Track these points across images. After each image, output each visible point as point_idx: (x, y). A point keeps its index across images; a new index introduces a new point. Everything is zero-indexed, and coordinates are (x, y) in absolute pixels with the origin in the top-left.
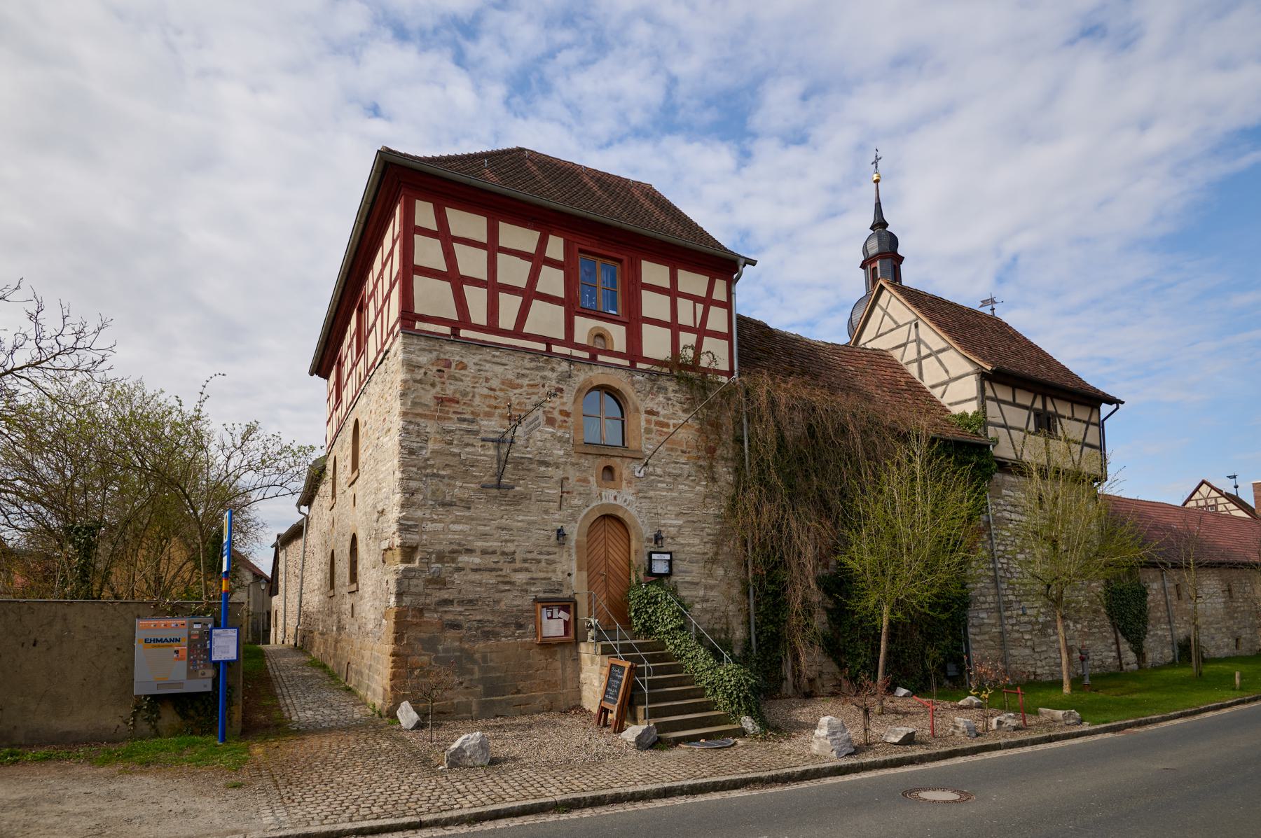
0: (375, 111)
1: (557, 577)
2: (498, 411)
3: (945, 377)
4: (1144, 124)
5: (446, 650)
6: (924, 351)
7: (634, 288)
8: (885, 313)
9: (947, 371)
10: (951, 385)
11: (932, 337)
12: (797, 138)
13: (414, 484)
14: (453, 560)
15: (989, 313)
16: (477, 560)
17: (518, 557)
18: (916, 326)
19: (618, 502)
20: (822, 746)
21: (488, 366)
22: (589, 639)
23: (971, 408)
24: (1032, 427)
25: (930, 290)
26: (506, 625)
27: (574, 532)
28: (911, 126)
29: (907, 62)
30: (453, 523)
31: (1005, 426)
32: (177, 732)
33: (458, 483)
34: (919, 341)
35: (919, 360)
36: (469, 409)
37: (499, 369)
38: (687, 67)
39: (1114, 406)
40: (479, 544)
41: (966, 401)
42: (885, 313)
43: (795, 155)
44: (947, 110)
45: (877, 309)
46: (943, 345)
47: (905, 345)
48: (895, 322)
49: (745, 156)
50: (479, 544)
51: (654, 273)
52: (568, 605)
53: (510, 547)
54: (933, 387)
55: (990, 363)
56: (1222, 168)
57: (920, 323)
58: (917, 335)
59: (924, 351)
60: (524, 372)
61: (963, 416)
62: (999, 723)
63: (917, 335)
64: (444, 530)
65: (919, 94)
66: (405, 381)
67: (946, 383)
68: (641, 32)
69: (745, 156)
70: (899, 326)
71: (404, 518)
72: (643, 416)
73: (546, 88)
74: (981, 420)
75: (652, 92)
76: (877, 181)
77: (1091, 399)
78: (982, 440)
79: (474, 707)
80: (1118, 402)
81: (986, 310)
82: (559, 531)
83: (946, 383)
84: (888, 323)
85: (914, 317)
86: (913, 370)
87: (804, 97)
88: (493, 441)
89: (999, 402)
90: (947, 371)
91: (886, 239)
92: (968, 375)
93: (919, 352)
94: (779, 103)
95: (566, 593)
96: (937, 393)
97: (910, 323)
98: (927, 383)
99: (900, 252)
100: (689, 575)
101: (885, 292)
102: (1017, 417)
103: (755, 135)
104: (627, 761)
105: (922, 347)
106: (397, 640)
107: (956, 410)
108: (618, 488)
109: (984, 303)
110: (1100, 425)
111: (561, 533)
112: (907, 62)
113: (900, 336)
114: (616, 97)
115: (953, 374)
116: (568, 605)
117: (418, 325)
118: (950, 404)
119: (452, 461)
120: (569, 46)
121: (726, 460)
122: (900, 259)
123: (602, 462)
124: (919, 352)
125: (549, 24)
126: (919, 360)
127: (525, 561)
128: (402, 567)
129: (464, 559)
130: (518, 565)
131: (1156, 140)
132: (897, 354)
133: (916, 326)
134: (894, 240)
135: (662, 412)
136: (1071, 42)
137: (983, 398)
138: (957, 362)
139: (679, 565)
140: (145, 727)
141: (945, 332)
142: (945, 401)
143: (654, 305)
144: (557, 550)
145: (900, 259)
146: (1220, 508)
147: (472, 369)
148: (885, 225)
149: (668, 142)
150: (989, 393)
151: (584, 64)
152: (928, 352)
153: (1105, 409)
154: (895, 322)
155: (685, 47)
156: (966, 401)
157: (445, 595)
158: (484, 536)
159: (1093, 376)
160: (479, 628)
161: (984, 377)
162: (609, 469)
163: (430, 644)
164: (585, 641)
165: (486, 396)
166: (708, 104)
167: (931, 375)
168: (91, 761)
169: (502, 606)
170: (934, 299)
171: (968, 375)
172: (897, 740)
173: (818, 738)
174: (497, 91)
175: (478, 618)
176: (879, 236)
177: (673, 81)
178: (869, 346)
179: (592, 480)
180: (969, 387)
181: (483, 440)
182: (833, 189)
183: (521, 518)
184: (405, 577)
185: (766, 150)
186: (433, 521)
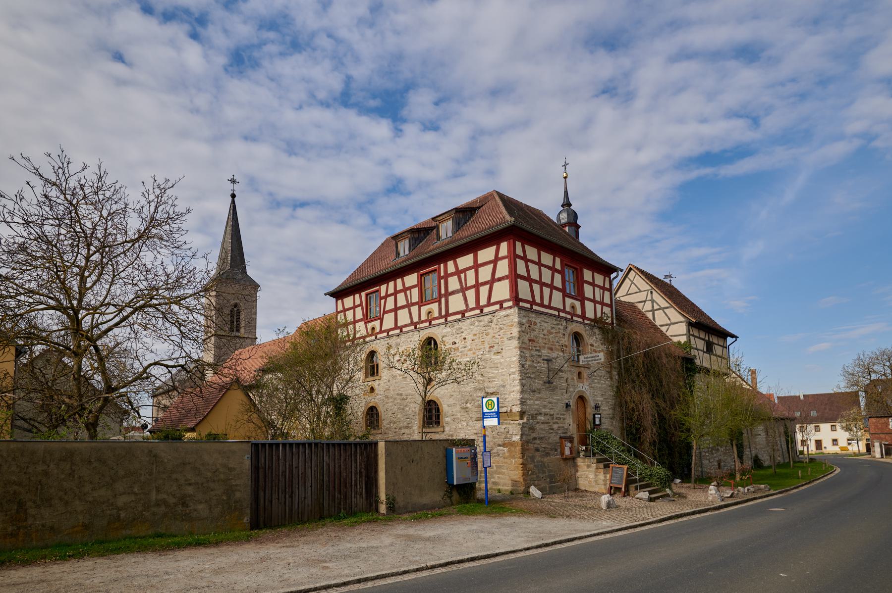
0: (119, 57)
1: (566, 426)
3: (669, 322)
4: (638, 148)
6: (656, 307)
7: (580, 283)
8: (632, 282)
11: (660, 300)
12: (431, 126)
13: (524, 382)
23: (683, 339)
25: (648, 272)
26: (552, 449)
27: (572, 403)
28: (502, 130)
29: (499, 92)
31: (696, 349)
32: (459, 503)
34: (653, 301)
35: (653, 311)
37: (546, 325)
38: (360, 73)
42: (632, 282)
43: (430, 137)
44: (525, 124)
46: (668, 305)
47: (644, 302)
49: (398, 132)
51: (587, 275)
52: (571, 439)
53: (552, 412)
54: (661, 326)
55: (694, 318)
56: (680, 177)
59: (656, 307)
61: (679, 342)
64: (535, 403)
65: (505, 112)
67: (669, 325)
68: (323, 42)
69: (398, 132)
70: (641, 291)
73: (255, 64)
74: (687, 346)
75: (336, 83)
78: (689, 356)
80: (737, 337)
81: (667, 281)
83: (669, 325)
86: (650, 315)
87: (436, 104)
89: (695, 336)
94: (421, 103)
95: (569, 434)
96: (664, 329)
100: (606, 425)
103: (404, 121)
107: (675, 339)
108: (583, 382)
109: (666, 277)
110: (727, 348)
111: (568, 405)
112: (499, 92)
113: (642, 296)
114: (306, 80)
115: (673, 320)
120: (273, 42)
124: (653, 307)
125: (261, 27)
126: (653, 311)
129: (539, 417)
130: (555, 420)
131: (644, 157)
132: (640, 306)
136: (597, 96)
137: (689, 335)
138: (674, 315)
139: (603, 420)
140: (448, 501)
142: (668, 334)
143: (588, 291)
146: (738, 384)
147: (539, 325)
149: (343, 111)
151: (282, 54)
153: (730, 340)
155: (357, 60)
157: (534, 435)
158: (545, 406)
159: (723, 322)
161: (690, 324)
162: (580, 373)
166: (374, 97)
167: (660, 319)
169: (550, 441)
174: (221, 60)
177: (349, 80)
178: (622, 299)
180: (682, 328)
182: (457, 161)
185: (411, 130)
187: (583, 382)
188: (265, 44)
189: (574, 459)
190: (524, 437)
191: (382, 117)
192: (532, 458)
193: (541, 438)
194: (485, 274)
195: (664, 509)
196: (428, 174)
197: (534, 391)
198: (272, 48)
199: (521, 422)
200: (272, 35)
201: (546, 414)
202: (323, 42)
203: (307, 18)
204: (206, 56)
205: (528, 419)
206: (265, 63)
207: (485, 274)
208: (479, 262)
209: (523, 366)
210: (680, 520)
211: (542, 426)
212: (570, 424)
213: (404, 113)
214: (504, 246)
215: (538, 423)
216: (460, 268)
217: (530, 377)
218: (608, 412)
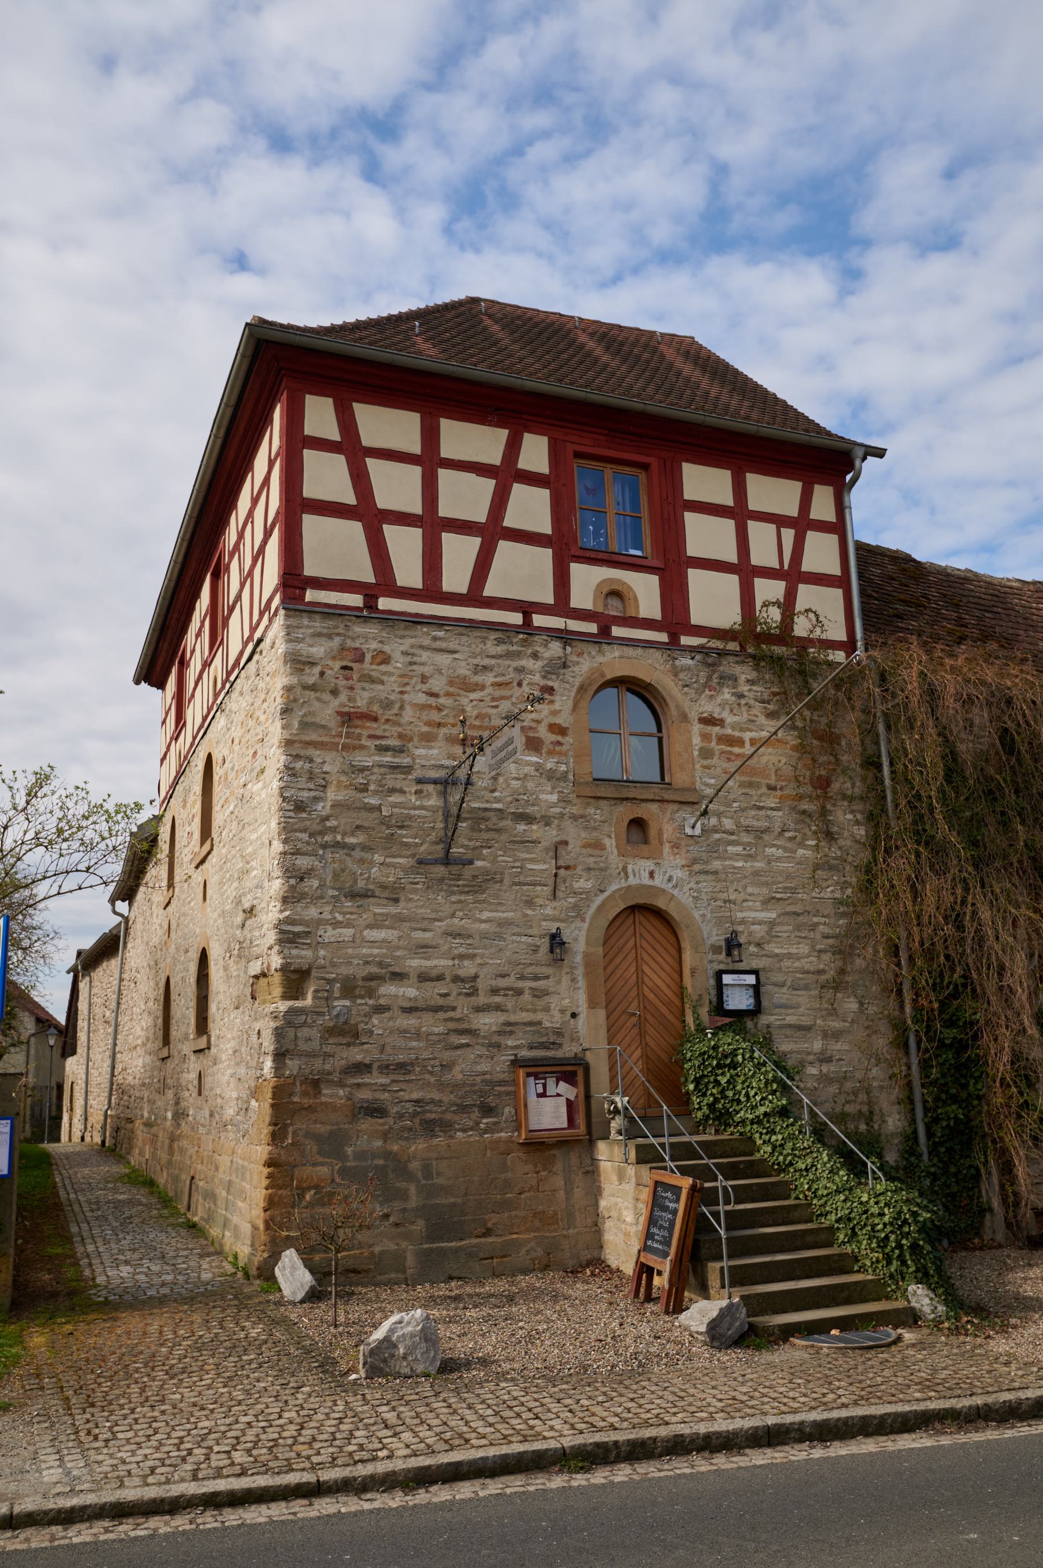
1: (552, 1020)
12: (942, 239)
13: (303, 862)
26: (463, 1109)
27: (580, 938)
38: (743, 148)
43: (939, 269)
52: (573, 1071)
53: (468, 968)
64: (356, 939)
69: (851, 278)
73: (511, 202)
75: (687, 191)
87: (950, 174)
94: (907, 186)
95: (569, 1050)
103: (866, 243)
111: (556, 941)
114: (624, 205)
125: (513, 103)
129: (389, 990)
130: (482, 999)
139: (774, 995)
149: (715, 266)
151: (570, 160)
155: (738, 116)
157: (357, 1055)
166: (783, 200)
169: (457, 1074)
174: (432, 215)
182: (1014, 318)
185: (891, 271)
187: (656, 856)
188: (530, 144)
189: (591, 1143)
190: (293, 1065)
191: (811, 254)
192: (333, 1144)
193: (401, 1067)
195: (787, 1382)
196: (936, 370)
198: (543, 152)
199: (283, 1006)
200: (540, 119)
201: (424, 978)
202: (664, 100)
203: (621, 53)
204: (401, 213)
205: (325, 998)
206: (533, 191)
208: (752, 525)
209: (300, 807)
210: (839, 1450)
212: (574, 1010)
213: (866, 221)
215: (380, 1009)
216: (805, 568)
218: (811, 963)
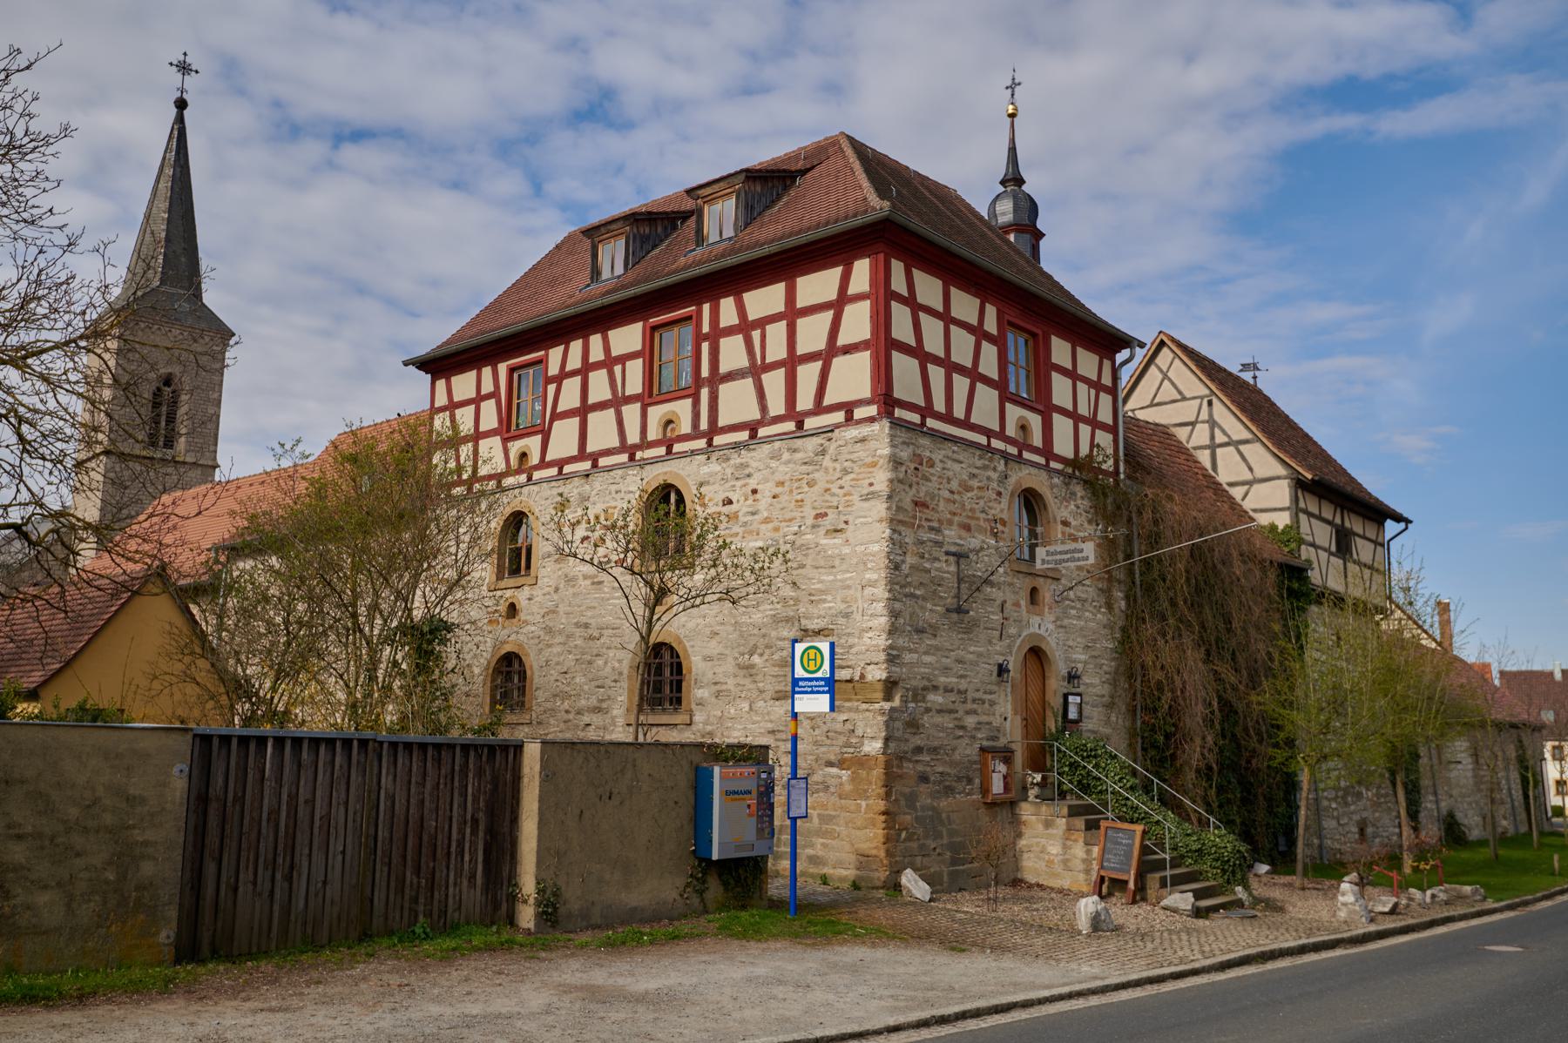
2: (956, 519)
3: (1248, 476)
5: (923, 808)
6: (1220, 438)
8: (1165, 376)
9: (1251, 469)
10: (1256, 486)
11: (1232, 425)
13: (897, 605)
14: (924, 700)
15: (1251, 382)
16: (940, 699)
17: (970, 695)
18: (1210, 403)
19: (1042, 632)
20: (1350, 912)
21: (949, 464)
22: (1031, 798)
23: (1282, 520)
24: (1333, 549)
26: (959, 779)
27: (1013, 664)
30: (926, 653)
32: (723, 907)
33: (929, 606)
34: (1213, 423)
35: (1213, 447)
36: (936, 516)
39: (1403, 525)
40: (942, 679)
41: (1275, 510)
42: (1165, 376)
45: (1153, 369)
47: (1193, 424)
48: (1180, 393)
50: (942, 679)
51: (1060, 351)
52: (1006, 755)
54: (1231, 484)
55: (1310, 468)
57: (1215, 400)
58: (1211, 415)
59: (1220, 438)
60: (975, 471)
61: (1273, 528)
62: (1433, 896)
63: (1211, 415)
64: (921, 661)
66: (891, 481)
67: (1250, 483)
70: (1184, 399)
71: (891, 647)
72: (1060, 527)
74: (1291, 535)
76: (1012, 116)
77: (1377, 513)
78: (1295, 562)
79: (946, 878)
80: (1408, 522)
81: (1247, 376)
82: (1000, 666)
83: (1250, 483)
84: (1168, 392)
85: (1207, 392)
86: (1204, 458)
88: (57, 346)
90: (1251, 469)
91: (1024, 204)
92: (1278, 478)
93: (1212, 437)
95: (1002, 742)
96: (1237, 492)
97: (1202, 398)
98: (1223, 477)
99: (1040, 225)
101: (1165, 350)
102: (1324, 535)
104: (1175, 936)
105: (1217, 431)
106: (888, 795)
107: (1264, 519)
108: (1041, 614)
109: (1245, 367)
111: (1002, 670)
113: (1187, 411)
115: (1259, 473)
116: (1006, 755)
117: (898, 412)
118: (1255, 511)
119: (925, 578)
121: (1119, 582)
122: (1039, 235)
123: (1028, 583)
124: (1212, 437)
126: (1213, 447)
127: (974, 701)
128: (887, 706)
129: (931, 697)
130: (969, 706)
132: (1182, 434)
133: (1210, 403)
134: (1033, 208)
135: (1074, 523)
137: (1296, 510)
138: (1263, 460)
141: (1252, 420)
144: (995, 688)
145: (1039, 235)
146: (1407, 635)
148: (1019, 181)
150: (1302, 505)
152: (1226, 439)
153: (1391, 527)
154: (1180, 393)
156: (1275, 510)
157: (917, 741)
159: (1376, 484)
160: (940, 782)
161: (1300, 485)
163: (911, 799)
164: (1026, 800)
165: (948, 500)
167: (1228, 469)
168: (796, 937)
170: (1205, 359)
171: (1278, 478)
172: (1387, 909)
173: (1344, 904)
175: (940, 769)
176: (1015, 198)
178: (1141, 415)
179: (1023, 603)
180: (1281, 493)
181: (947, 553)
183: (972, 649)
184: (891, 718)
186: (911, 651)
194: (812, 333)
197: (920, 631)
201: (948, 690)
207: (812, 333)
211: (938, 719)
214: (862, 270)
215: (928, 710)
217: (912, 595)
